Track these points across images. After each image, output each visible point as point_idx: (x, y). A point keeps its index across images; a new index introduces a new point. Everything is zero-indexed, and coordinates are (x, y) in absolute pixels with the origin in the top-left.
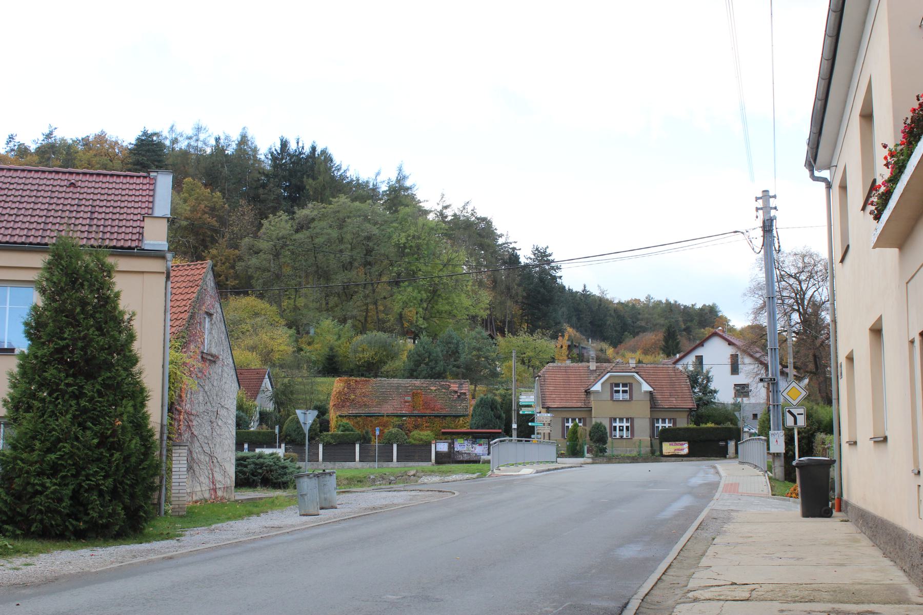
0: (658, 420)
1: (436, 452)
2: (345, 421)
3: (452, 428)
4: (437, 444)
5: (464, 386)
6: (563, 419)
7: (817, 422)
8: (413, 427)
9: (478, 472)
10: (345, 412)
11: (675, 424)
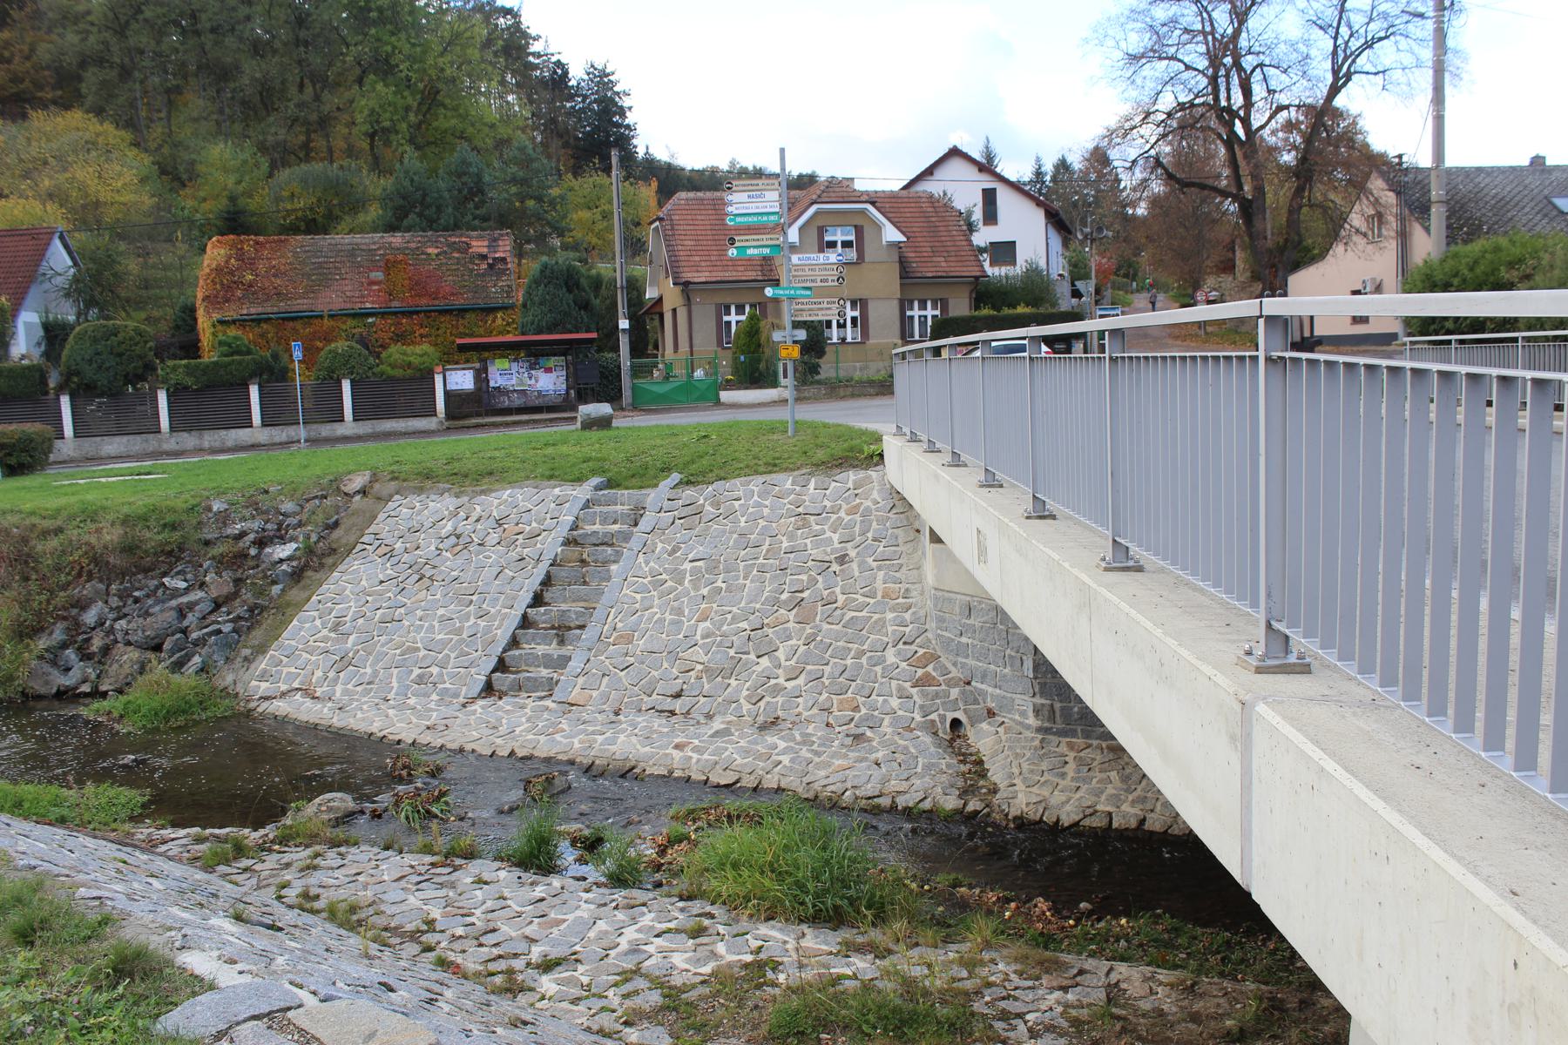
0: (911, 302)
1: (447, 394)
2: (233, 332)
3: (481, 336)
4: (448, 373)
5: (500, 243)
6: (718, 306)
8: (391, 339)
9: (594, 472)
10: (231, 313)
11: (944, 309)
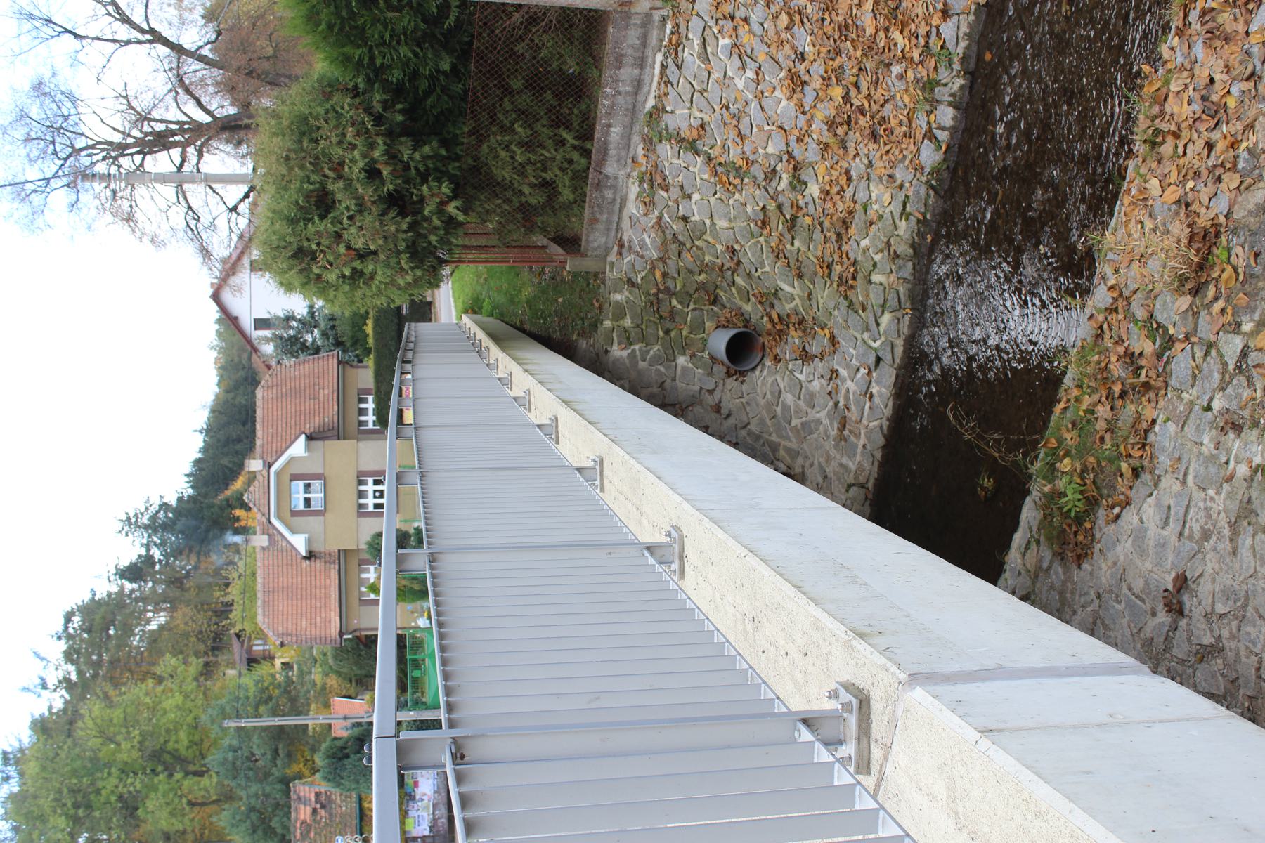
0: (361, 423)
5: (302, 794)
7: (328, 97)
11: (368, 392)
